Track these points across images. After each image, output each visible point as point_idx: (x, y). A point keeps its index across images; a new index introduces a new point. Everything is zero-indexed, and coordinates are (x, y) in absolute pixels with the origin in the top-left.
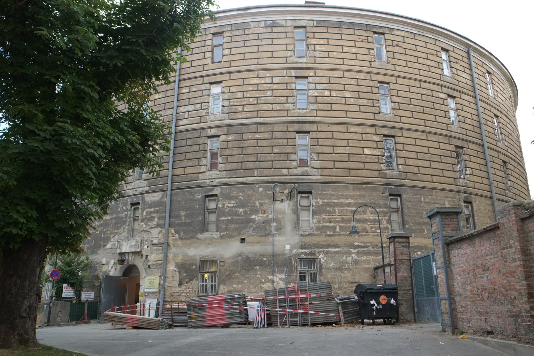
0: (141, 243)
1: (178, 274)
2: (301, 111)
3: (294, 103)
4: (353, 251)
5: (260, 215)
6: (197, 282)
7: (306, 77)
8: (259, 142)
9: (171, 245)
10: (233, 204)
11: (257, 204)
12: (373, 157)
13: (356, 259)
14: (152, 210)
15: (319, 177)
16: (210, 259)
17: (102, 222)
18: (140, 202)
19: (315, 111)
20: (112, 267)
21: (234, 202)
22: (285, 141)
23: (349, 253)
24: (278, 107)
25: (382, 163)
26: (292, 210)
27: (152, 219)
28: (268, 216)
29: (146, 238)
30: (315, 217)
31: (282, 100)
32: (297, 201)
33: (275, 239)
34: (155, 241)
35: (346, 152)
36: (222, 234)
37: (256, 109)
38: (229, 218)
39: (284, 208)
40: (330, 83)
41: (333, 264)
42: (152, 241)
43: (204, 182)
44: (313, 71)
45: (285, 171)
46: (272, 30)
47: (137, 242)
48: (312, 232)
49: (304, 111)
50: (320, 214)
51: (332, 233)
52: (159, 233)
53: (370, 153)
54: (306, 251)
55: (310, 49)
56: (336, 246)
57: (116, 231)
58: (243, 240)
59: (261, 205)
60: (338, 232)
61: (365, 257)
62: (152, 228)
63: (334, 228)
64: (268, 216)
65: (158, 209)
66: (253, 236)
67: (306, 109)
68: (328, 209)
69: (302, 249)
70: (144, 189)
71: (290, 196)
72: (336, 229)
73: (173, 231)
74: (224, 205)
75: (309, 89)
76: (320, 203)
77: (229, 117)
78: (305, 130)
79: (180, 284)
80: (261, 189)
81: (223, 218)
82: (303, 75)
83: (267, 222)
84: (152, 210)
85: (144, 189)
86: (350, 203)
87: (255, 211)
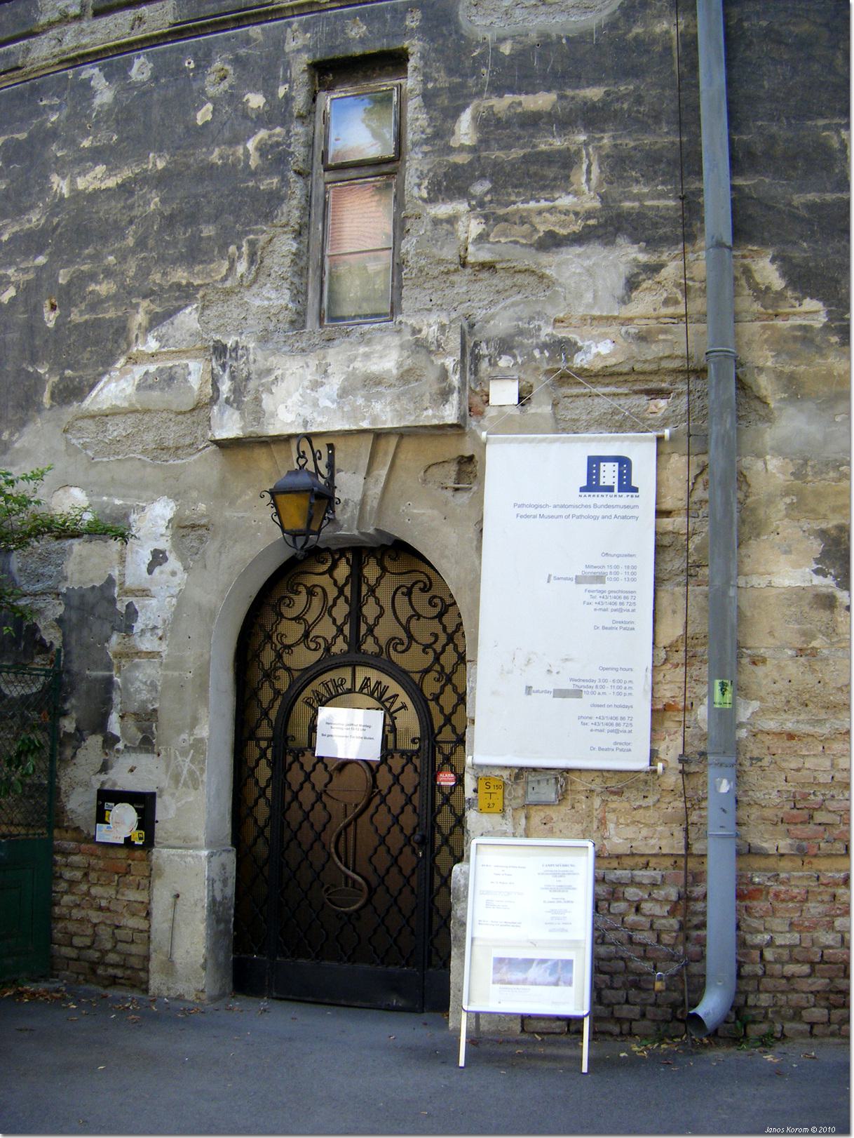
9: (765, 385)
20: (158, 558)
34: (599, 350)
42: (563, 347)
62: (552, 242)
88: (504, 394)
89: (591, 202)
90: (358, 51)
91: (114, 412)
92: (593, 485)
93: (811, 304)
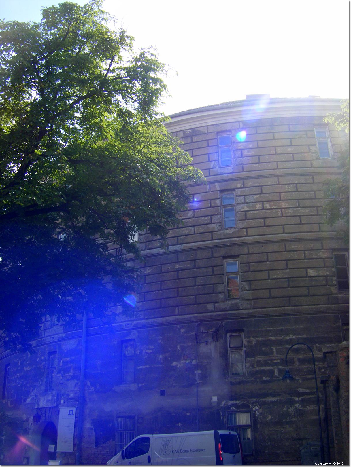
0: (57, 398)
1: (94, 434)
2: (229, 231)
3: (220, 222)
4: (296, 399)
5: (182, 362)
6: (114, 442)
7: (234, 190)
8: (179, 274)
9: (87, 399)
10: (152, 349)
11: (179, 348)
12: (320, 278)
13: (300, 410)
14: (68, 359)
15: (251, 311)
16: (127, 414)
17: (23, 374)
18: (57, 350)
19: (245, 230)
20: (31, 424)
21: (152, 347)
22: (210, 270)
23: (291, 403)
24: (201, 229)
25: (333, 286)
26: (220, 353)
27: (67, 370)
28: (191, 362)
29: (63, 392)
30: (248, 359)
31: (206, 220)
32: (226, 342)
33: (199, 389)
34: (72, 395)
35: (285, 277)
36: (140, 385)
37: (176, 235)
38: (148, 366)
39: (209, 351)
40: (262, 193)
41: (270, 417)
42: (68, 395)
43: (121, 325)
44: (241, 182)
45: (210, 307)
46: (192, 140)
47: (53, 396)
48: (244, 379)
49: (233, 231)
50: (254, 356)
51: (268, 379)
52: (75, 386)
53: (316, 274)
54: (238, 402)
55: (237, 155)
56: (274, 395)
57: (35, 384)
58: (163, 393)
59: (183, 349)
60: (276, 377)
61: (312, 406)
62: (68, 380)
63: (272, 372)
64: (191, 362)
65: (73, 358)
66: (174, 386)
67: (235, 228)
68: (263, 349)
69: (232, 400)
70: (60, 335)
71: (216, 336)
72: (274, 373)
73: (89, 384)
74: (141, 351)
75: (237, 204)
76: (254, 343)
77: (146, 246)
78: (233, 254)
79: (97, 445)
80: (182, 330)
81: (141, 367)
82: (229, 187)
83: (190, 369)
84: (68, 359)
85: (60, 335)
86: (291, 339)
87: (177, 358)
88: (62, 401)
89: (72, 374)
90: (52, 351)
91: (29, 403)
92: (69, 414)
93: (93, 388)
